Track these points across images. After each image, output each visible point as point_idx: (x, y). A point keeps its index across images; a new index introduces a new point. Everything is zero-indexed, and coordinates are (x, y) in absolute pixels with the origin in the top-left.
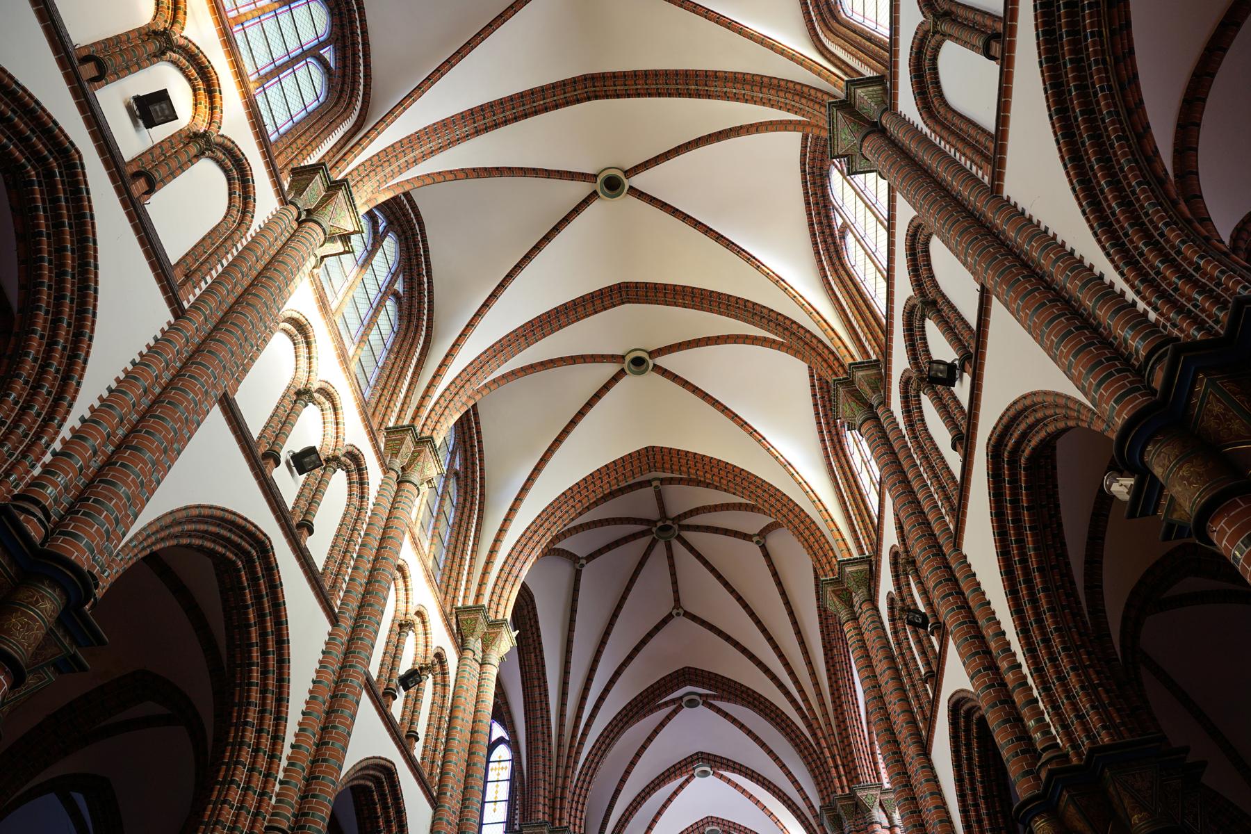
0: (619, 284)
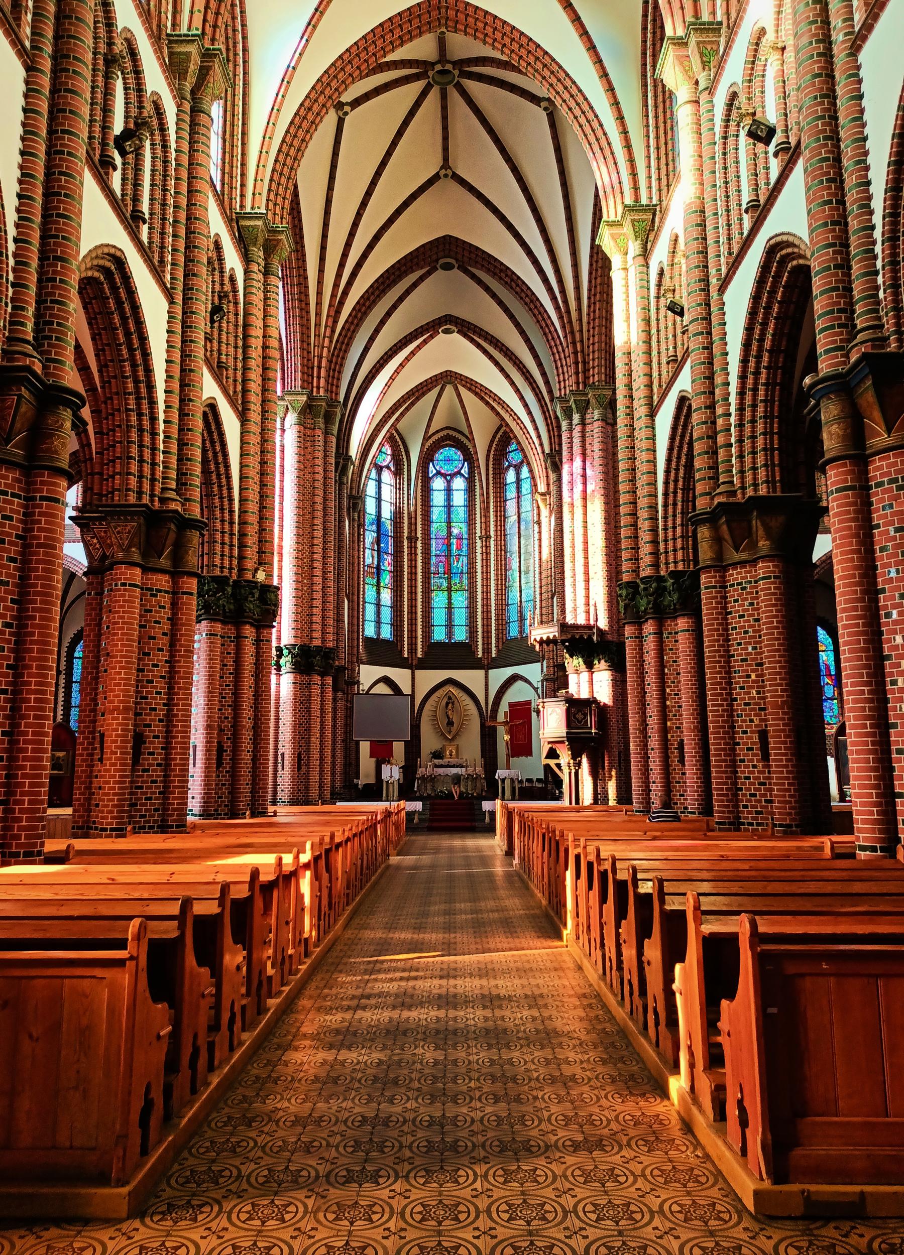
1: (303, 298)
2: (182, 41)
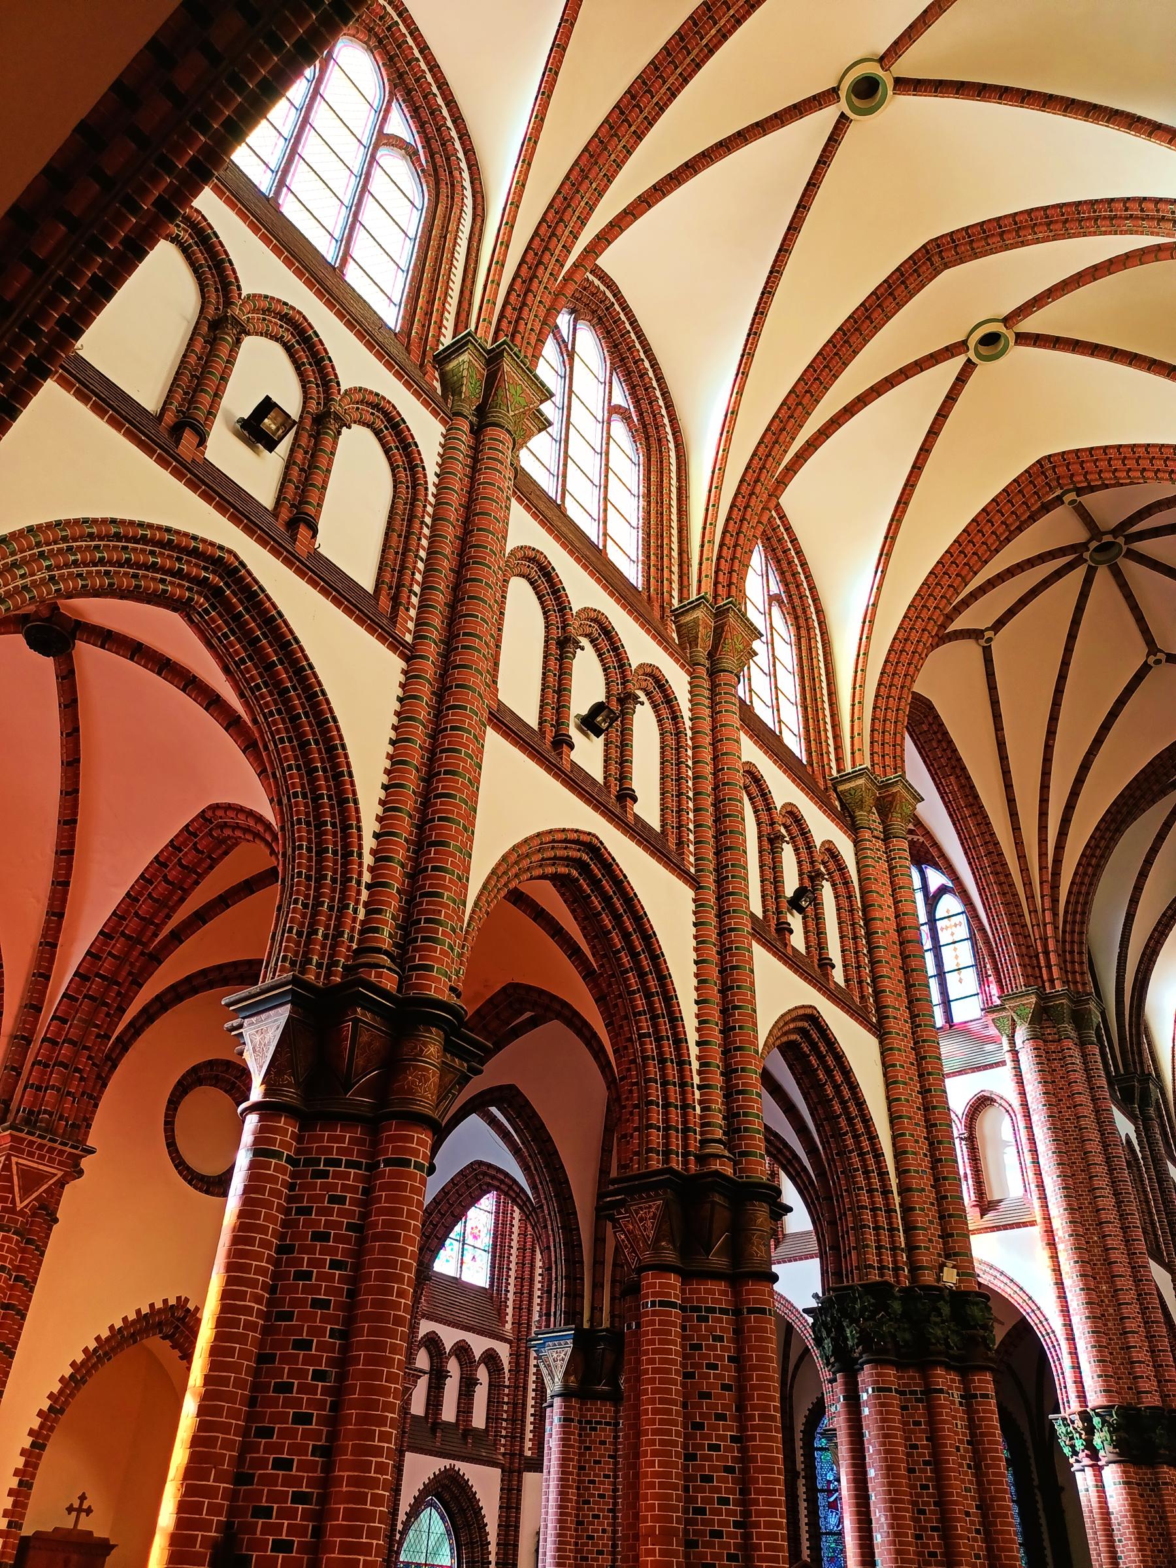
0: (924, 246)
1: (999, 869)
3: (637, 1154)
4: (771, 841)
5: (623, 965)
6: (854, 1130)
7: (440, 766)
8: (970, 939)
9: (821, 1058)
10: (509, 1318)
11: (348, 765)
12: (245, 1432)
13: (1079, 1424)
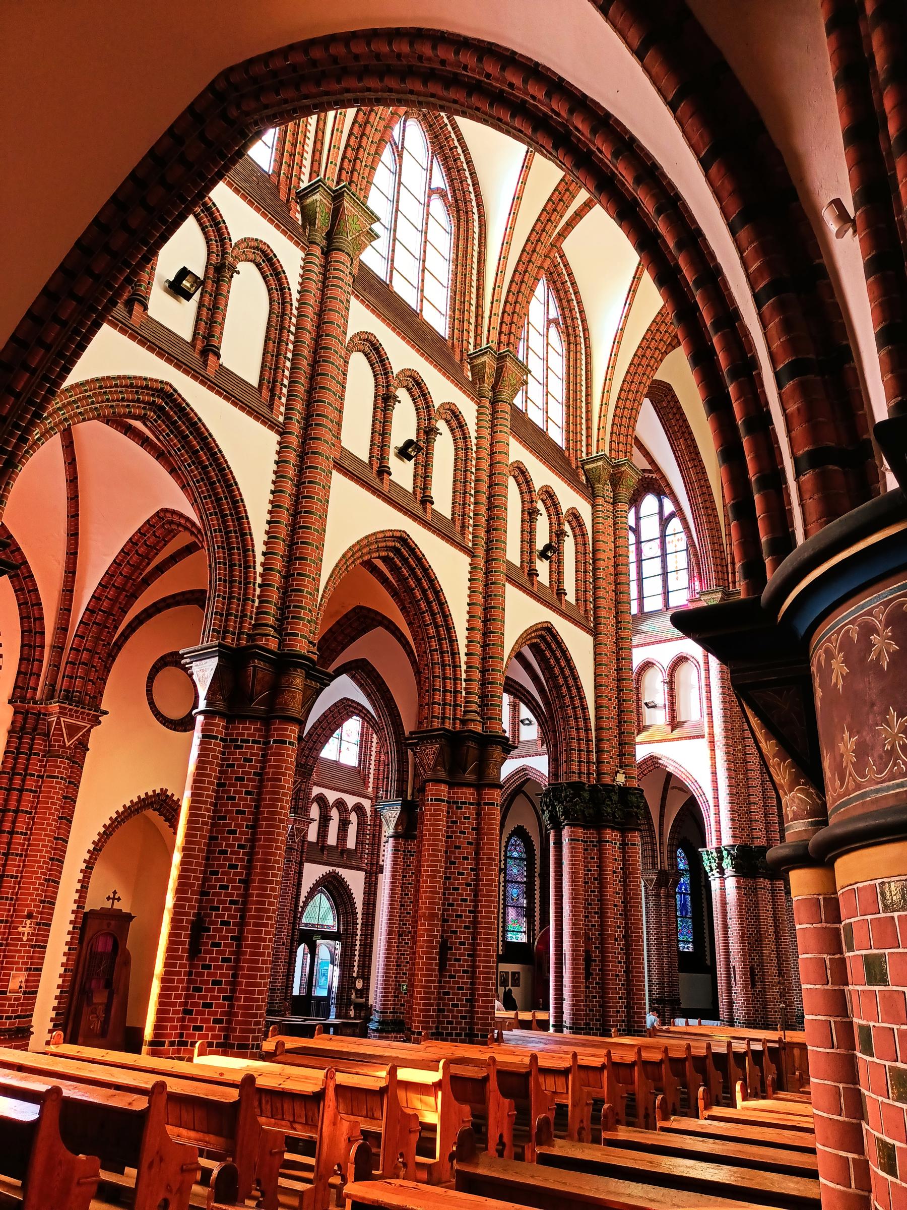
1: (708, 504)
2: (478, 356)
3: (426, 718)
4: (530, 514)
5: (421, 609)
6: (571, 694)
7: (302, 507)
8: (687, 550)
9: (553, 652)
10: (371, 785)
11: (246, 512)
12: (205, 872)
13: (715, 854)
